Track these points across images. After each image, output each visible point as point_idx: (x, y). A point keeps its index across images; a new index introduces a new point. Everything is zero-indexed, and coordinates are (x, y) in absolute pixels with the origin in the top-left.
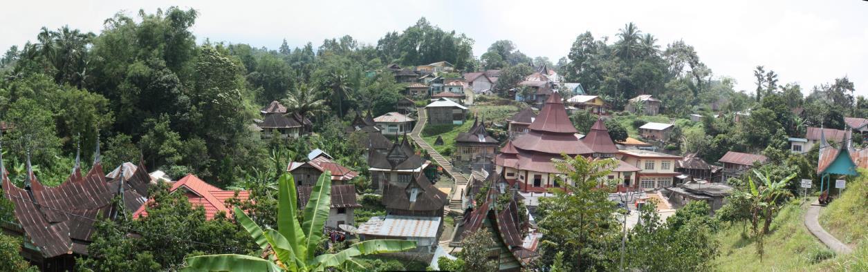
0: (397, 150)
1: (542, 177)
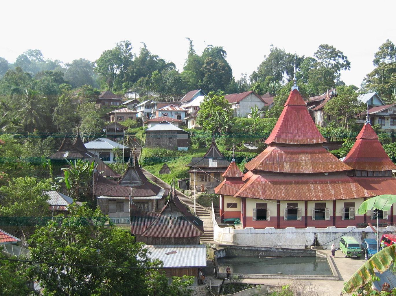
0: (130, 174)
1: (269, 206)
